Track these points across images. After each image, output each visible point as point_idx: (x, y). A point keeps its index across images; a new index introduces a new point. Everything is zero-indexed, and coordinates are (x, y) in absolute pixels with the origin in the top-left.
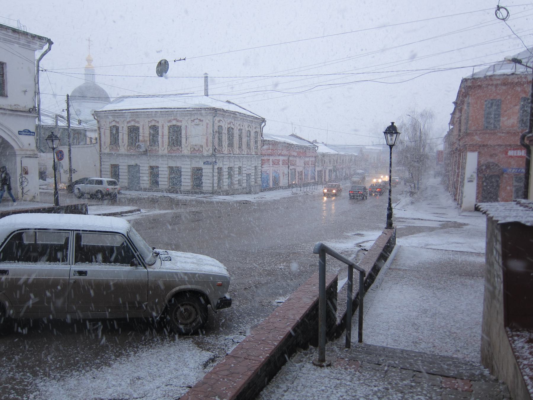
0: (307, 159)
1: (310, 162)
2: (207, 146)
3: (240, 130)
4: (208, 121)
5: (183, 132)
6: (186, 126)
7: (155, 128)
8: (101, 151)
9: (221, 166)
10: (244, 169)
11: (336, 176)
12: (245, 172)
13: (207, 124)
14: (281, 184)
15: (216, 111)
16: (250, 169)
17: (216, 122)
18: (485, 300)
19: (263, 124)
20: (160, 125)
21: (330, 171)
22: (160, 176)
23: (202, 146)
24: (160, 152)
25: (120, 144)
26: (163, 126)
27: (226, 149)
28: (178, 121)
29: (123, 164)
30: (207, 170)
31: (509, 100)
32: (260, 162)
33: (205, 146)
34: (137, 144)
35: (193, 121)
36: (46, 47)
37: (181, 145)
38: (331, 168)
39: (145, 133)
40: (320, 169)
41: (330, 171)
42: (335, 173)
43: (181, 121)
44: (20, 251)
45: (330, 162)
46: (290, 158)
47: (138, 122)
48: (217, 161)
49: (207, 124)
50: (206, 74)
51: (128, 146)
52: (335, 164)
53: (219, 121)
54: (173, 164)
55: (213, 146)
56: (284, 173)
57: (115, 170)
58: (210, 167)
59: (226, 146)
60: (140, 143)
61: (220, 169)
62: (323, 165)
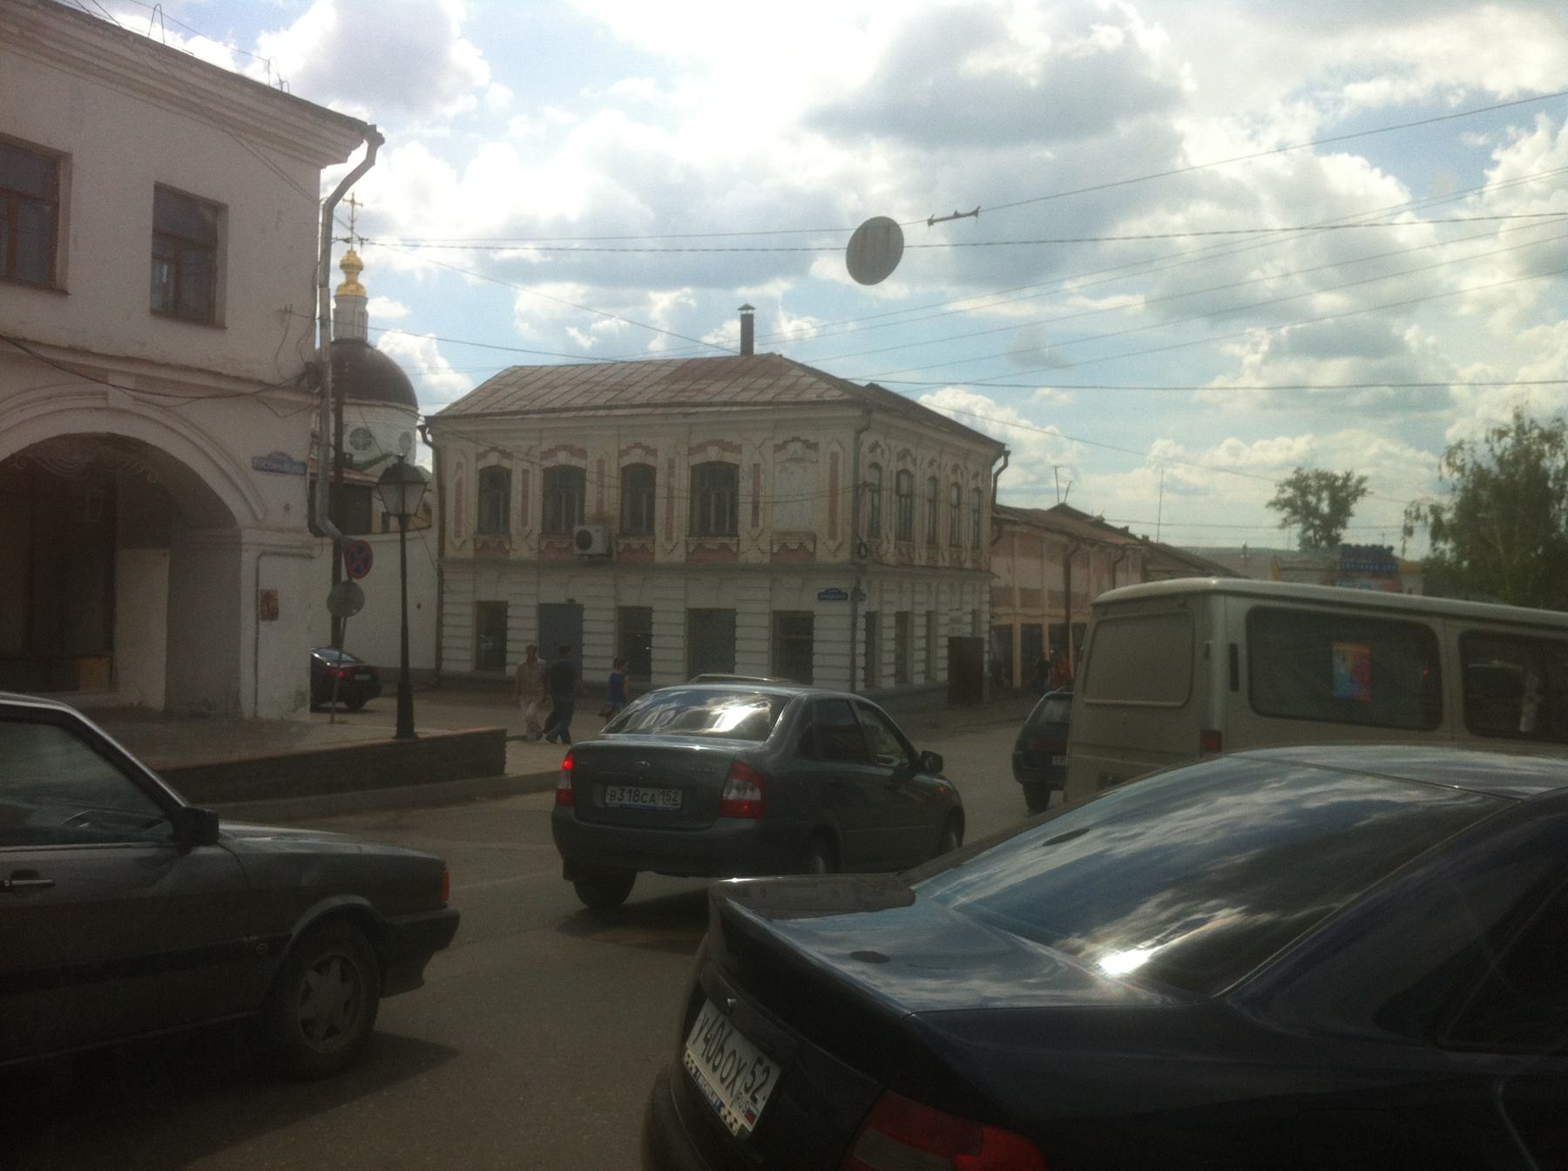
3: (934, 480)
4: (835, 447)
5: (745, 486)
6: (756, 466)
7: (639, 480)
8: (441, 552)
9: (875, 608)
13: (834, 456)
15: (869, 412)
17: (865, 449)
19: (1000, 463)
20: (660, 463)
22: (655, 641)
24: (660, 557)
25: (513, 530)
26: (671, 466)
27: (892, 547)
28: (725, 446)
29: (524, 602)
31: (1234, 452)
32: (987, 597)
34: (577, 529)
35: (779, 448)
36: (358, 155)
37: (734, 533)
43: (737, 449)
47: (582, 453)
48: (864, 588)
50: (747, 307)
53: (874, 448)
54: (705, 599)
55: (855, 533)
57: (492, 618)
58: (844, 608)
59: (892, 536)
60: (590, 528)
61: (871, 618)
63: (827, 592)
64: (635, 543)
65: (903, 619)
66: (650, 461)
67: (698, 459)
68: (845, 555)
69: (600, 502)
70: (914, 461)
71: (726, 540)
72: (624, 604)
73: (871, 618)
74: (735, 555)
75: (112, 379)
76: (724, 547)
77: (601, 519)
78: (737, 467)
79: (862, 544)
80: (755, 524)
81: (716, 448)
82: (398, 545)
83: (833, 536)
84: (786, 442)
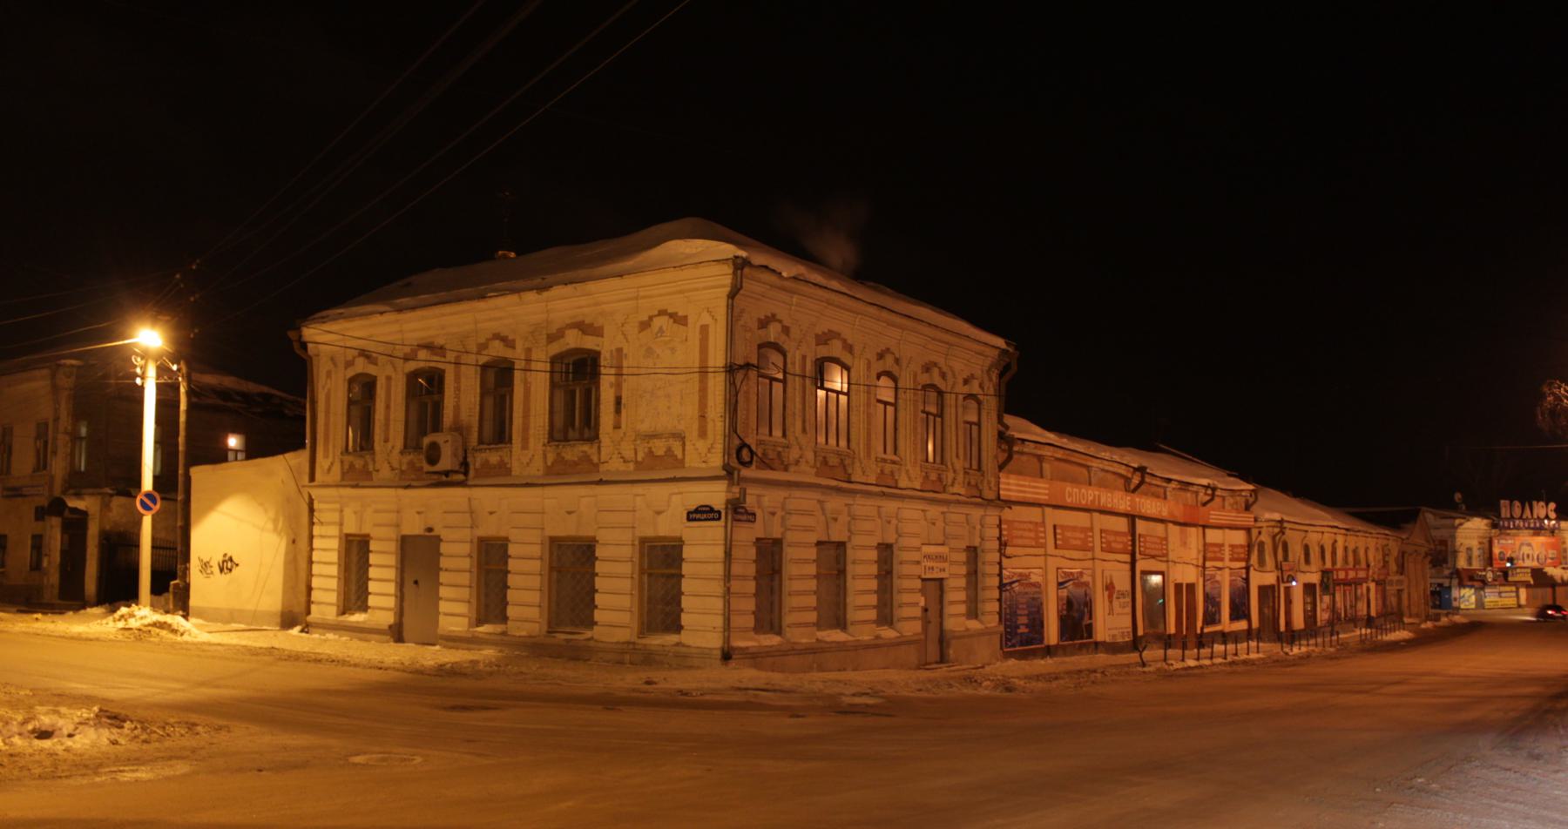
0: (1213, 536)
1: (1227, 550)
2: (703, 434)
4: (706, 319)
6: (620, 350)
10: (905, 556)
11: (1333, 608)
12: (916, 570)
13: (704, 329)
14: (1102, 633)
16: (940, 558)
18: (482, 297)
21: (1309, 588)
23: (681, 438)
30: (704, 548)
33: (692, 434)
38: (1314, 578)
39: (463, 397)
40: (1270, 579)
41: (1309, 588)
42: (1327, 599)
44: (1282, 628)
45: (1307, 555)
46: (1141, 527)
49: (704, 329)
51: (402, 453)
52: (1328, 565)
56: (1110, 587)
61: (770, 555)
62: (1279, 567)
63: (697, 511)
64: (494, 458)
65: (834, 556)
66: (509, 354)
67: (556, 348)
68: (716, 461)
69: (457, 408)
70: (786, 330)
71: (586, 448)
72: (406, 531)
73: (770, 555)
74: (596, 466)
75: (1095, 464)
76: (586, 458)
77: (459, 429)
78: (599, 353)
79: (744, 445)
80: (617, 426)
81: (575, 331)
82: (1128, 567)
83: (703, 434)
84: (651, 318)
